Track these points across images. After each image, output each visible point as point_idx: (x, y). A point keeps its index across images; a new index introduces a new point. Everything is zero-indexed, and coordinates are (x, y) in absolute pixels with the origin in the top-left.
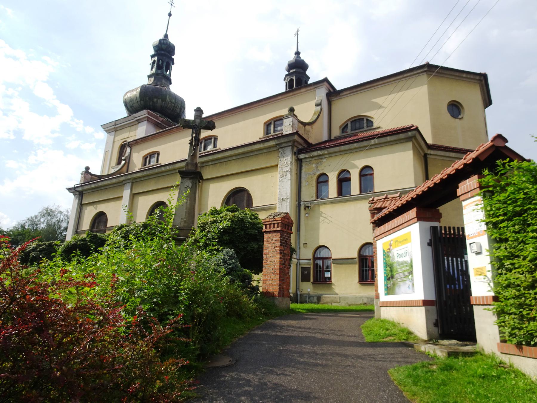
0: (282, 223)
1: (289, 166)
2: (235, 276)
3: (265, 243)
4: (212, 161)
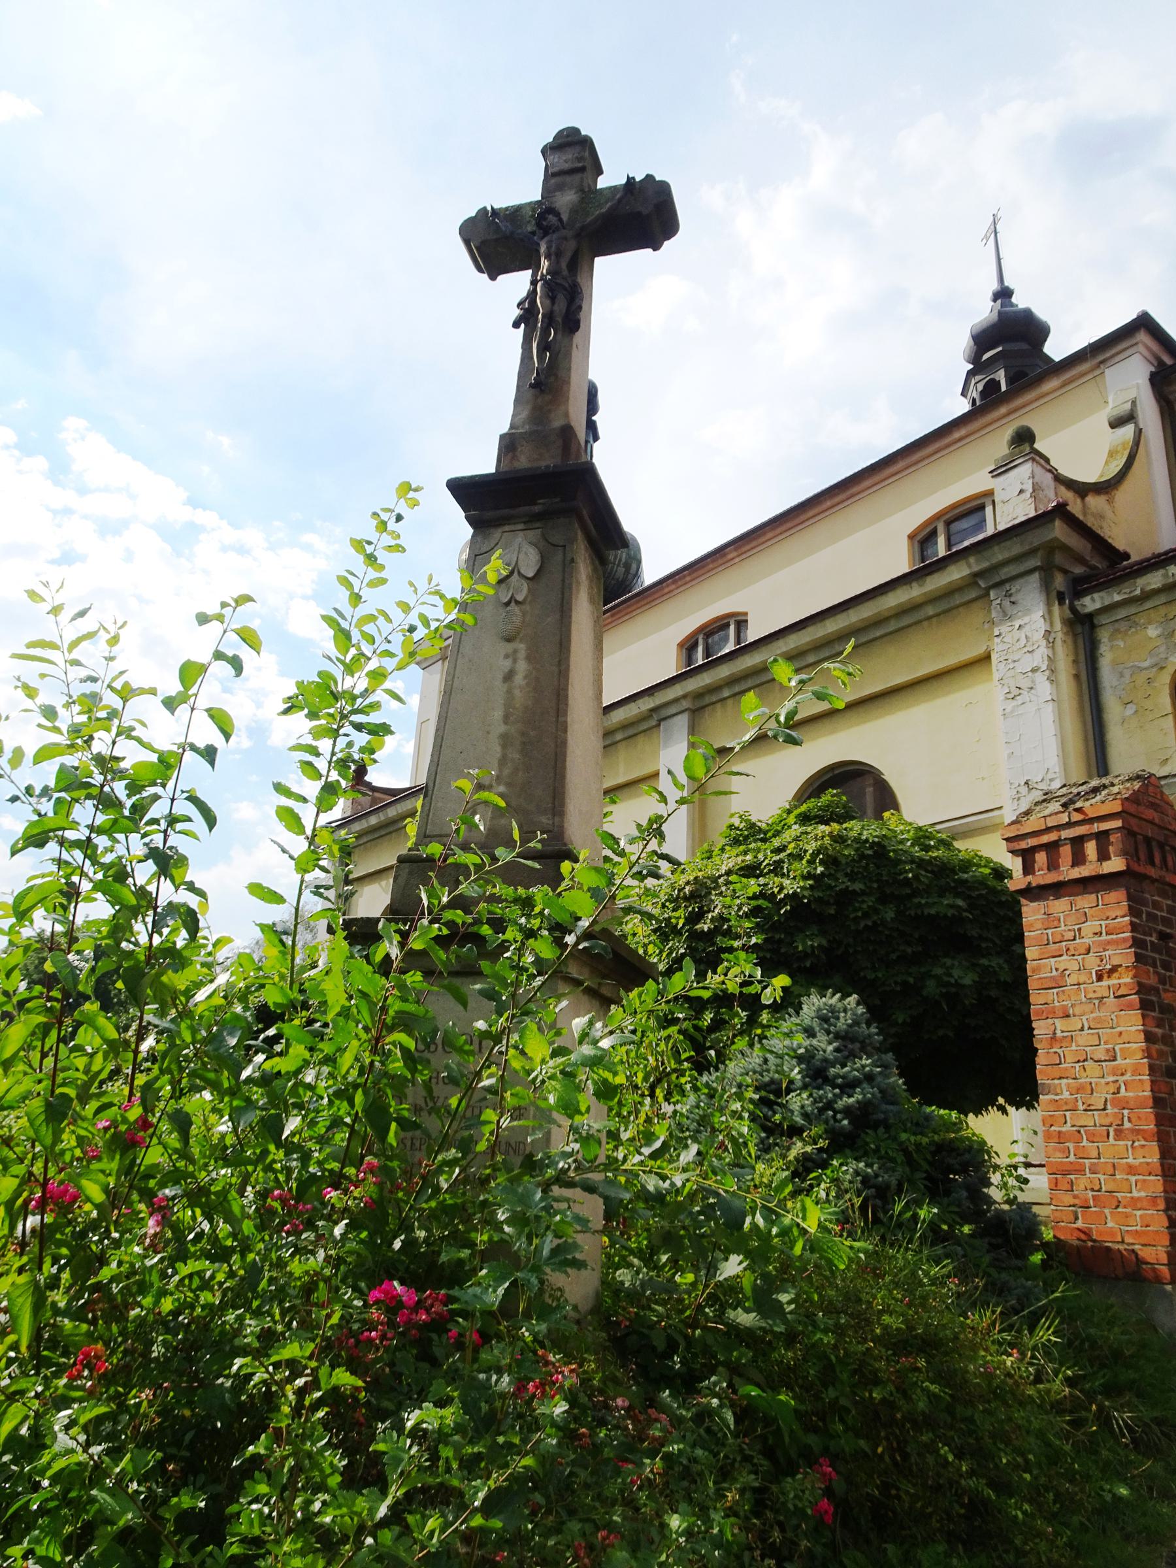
0: (1127, 830)
1: (1043, 651)
2: (886, 1161)
3: (1031, 953)
4: (732, 681)
